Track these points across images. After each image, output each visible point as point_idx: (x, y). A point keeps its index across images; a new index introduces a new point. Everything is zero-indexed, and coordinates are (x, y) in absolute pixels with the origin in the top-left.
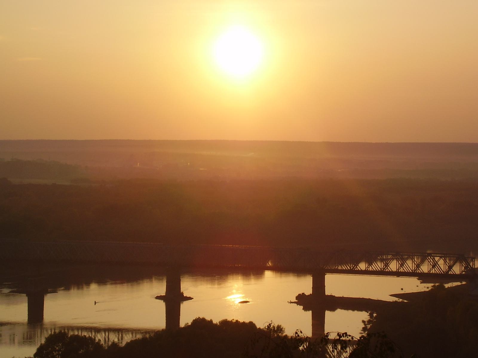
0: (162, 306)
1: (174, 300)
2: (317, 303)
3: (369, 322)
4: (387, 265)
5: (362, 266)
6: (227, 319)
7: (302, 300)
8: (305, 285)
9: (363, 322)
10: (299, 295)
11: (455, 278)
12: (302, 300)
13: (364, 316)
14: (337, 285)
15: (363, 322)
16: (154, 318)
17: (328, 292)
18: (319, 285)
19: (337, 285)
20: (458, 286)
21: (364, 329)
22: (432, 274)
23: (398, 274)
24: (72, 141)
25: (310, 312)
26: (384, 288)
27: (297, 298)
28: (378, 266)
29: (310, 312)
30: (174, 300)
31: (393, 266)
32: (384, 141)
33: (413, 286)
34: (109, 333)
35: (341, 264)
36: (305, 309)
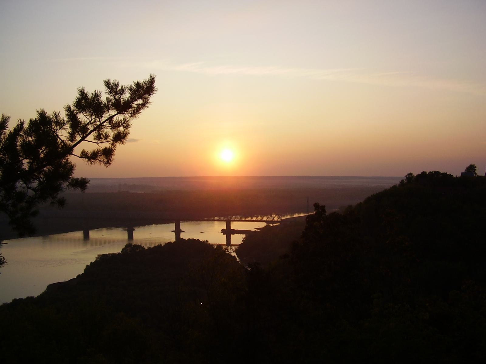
0: (174, 234)
1: (178, 231)
2: (228, 232)
3: (245, 238)
4: (262, 218)
5: (254, 219)
6: (207, 241)
7: (223, 231)
8: (224, 226)
9: (243, 238)
10: (222, 229)
11: (277, 222)
12: (223, 231)
13: (244, 236)
14: (235, 226)
15: (243, 238)
16: (172, 238)
17: (232, 228)
18: (228, 226)
19: (235, 226)
20: (278, 225)
21: (242, 241)
22: (279, 221)
23: (256, 221)
24: (174, 177)
25: (225, 235)
26: (252, 226)
27: (222, 230)
28: (249, 219)
29: (225, 235)
30: (178, 231)
31: (254, 219)
32: (268, 175)
33: (263, 225)
34: (73, 154)
35: (246, 218)
36: (224, 234)
